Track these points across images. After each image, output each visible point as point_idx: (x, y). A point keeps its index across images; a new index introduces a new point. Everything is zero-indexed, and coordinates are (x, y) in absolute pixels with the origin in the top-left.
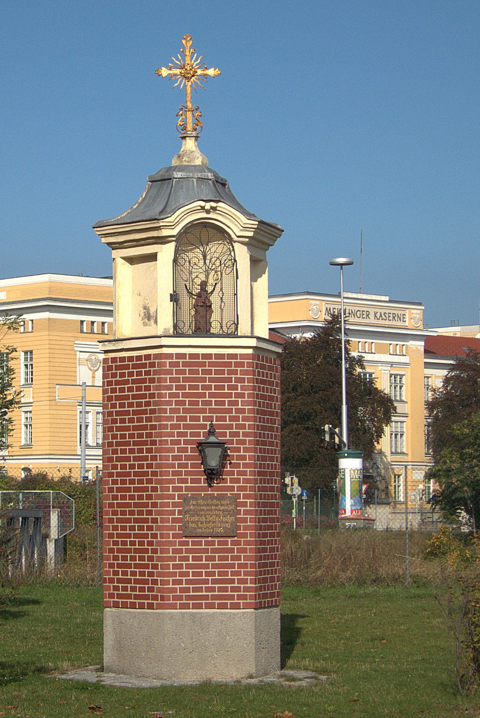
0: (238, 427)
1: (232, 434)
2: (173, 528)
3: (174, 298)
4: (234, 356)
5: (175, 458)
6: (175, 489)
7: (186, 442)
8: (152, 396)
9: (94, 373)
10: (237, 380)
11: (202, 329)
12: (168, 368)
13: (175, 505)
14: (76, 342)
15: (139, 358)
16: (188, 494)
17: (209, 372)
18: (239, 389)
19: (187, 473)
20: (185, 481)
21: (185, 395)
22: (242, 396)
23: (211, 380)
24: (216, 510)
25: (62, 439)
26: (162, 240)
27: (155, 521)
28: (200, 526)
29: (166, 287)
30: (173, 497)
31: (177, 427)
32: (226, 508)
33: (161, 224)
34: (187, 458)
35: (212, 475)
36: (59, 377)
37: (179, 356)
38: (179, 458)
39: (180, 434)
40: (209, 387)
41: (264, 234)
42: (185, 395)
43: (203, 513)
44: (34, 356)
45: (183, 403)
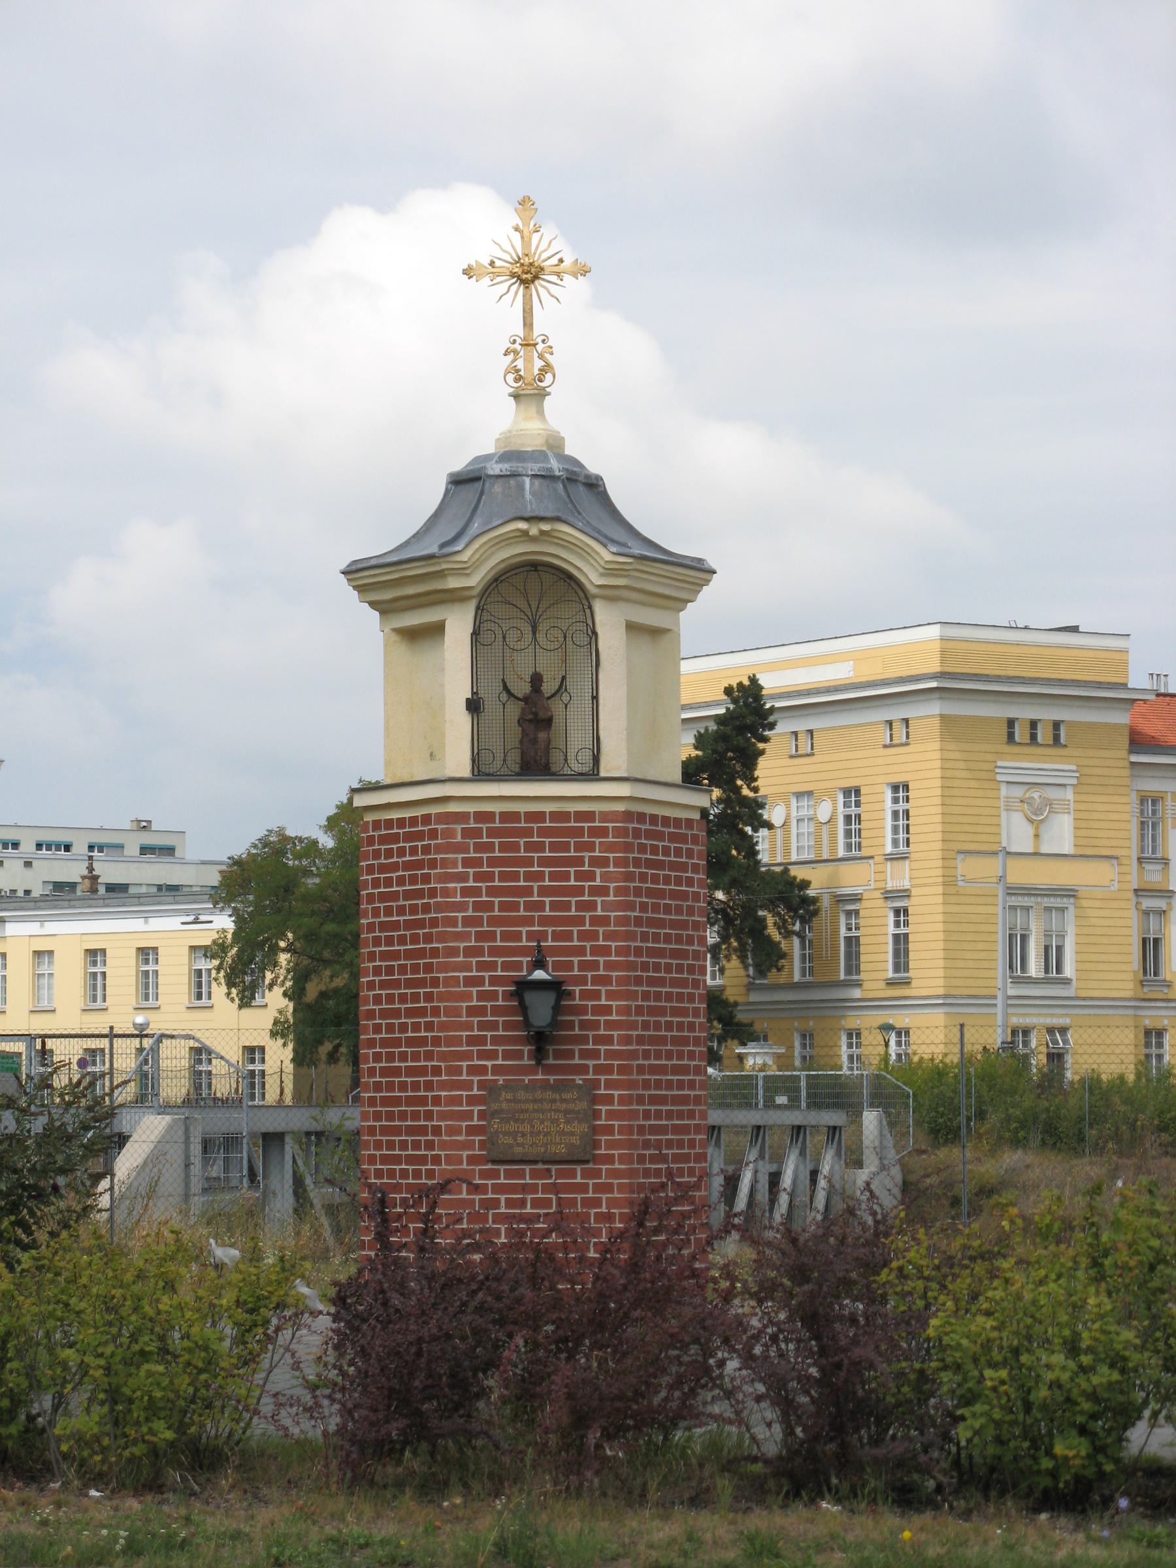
0: (596, 951)
1: (583, 966)
2: (468, 1145)
3: (474, 706)
4: (588, 816)
5: (471, 1011)
6: (472, 1070)
7: (494, 981)
8: (433, 893)
9: (1037, 828)
10: (594, 862)
11: (536, 763)
12: (459, 839)
13: (472, 1100)
14: (999, 764)
15: (413, 821)
16: (498, 1080)
17: (539, 847)
18: (598, 879)
19: (496, 1040)
20: (492, 1055)
21: (492, 891)
22: (603, 891)
23: (543, 862)
24: (551, 1110)
25: (971, 964)
26: (454, 597)
27: (437, 1131)
28: (520, 1140)
29: (459, 687)
30: (468, 1086)
31: (478, 951)
32: (571, 1106)
33: (444, 566)
34: (496, 1011)
35: (541, 1041)
36: (962, 837)
37: (481, 817)
38: (480, 1011)
39: (482, 966)
40: (539, 876)
41: (677, 584)
42: (492, 891)
43: (526, 1116)
44: (863, 799)
45: (489, 906)
